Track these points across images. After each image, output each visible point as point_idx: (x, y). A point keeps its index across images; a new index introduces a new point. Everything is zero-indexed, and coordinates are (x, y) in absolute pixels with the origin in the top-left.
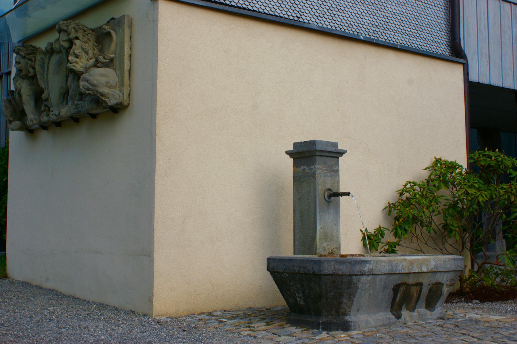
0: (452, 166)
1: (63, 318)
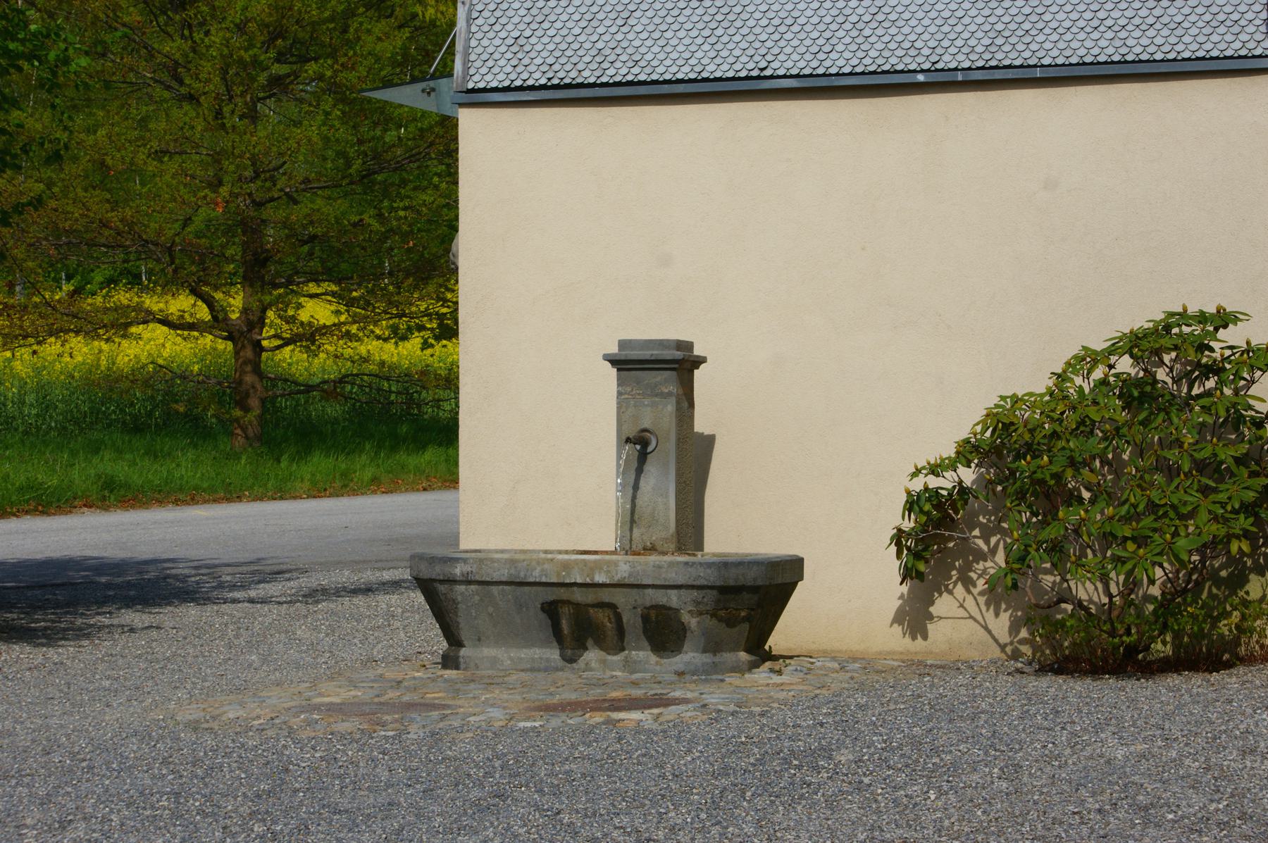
1: (728, 727)
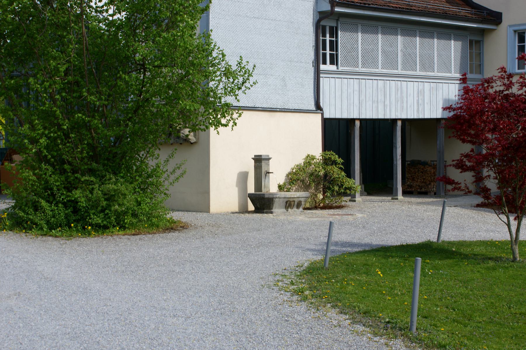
0: (313, 158)
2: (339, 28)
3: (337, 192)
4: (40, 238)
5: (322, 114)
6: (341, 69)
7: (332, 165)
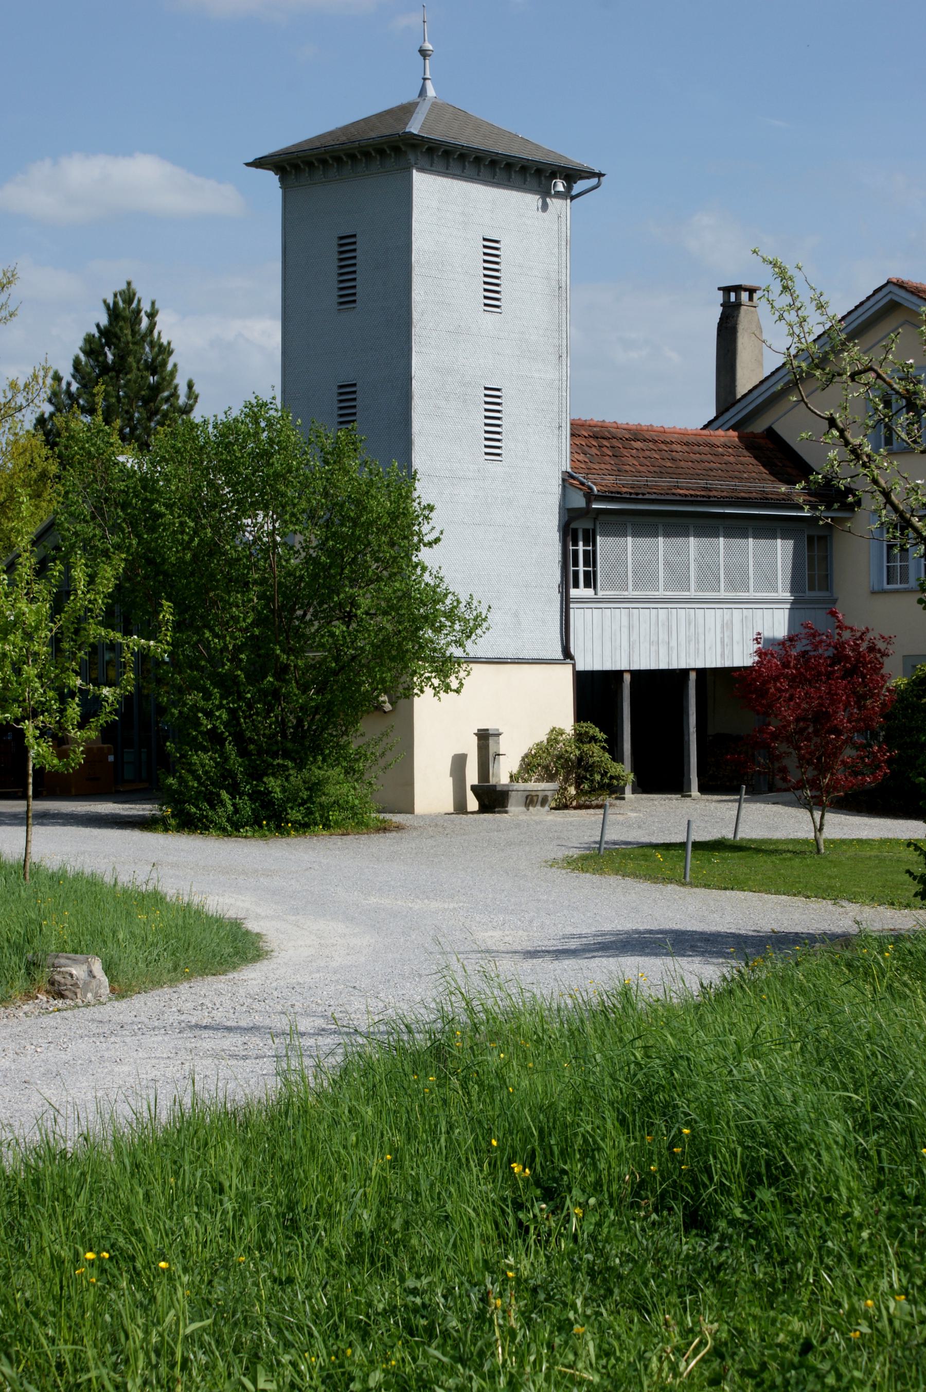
0: (561, 733)
2: (598, 530)
3: (598, 783)
4: (226, 839)
5: (574, 666)
6: (601, 594)
7: (590, 742)
